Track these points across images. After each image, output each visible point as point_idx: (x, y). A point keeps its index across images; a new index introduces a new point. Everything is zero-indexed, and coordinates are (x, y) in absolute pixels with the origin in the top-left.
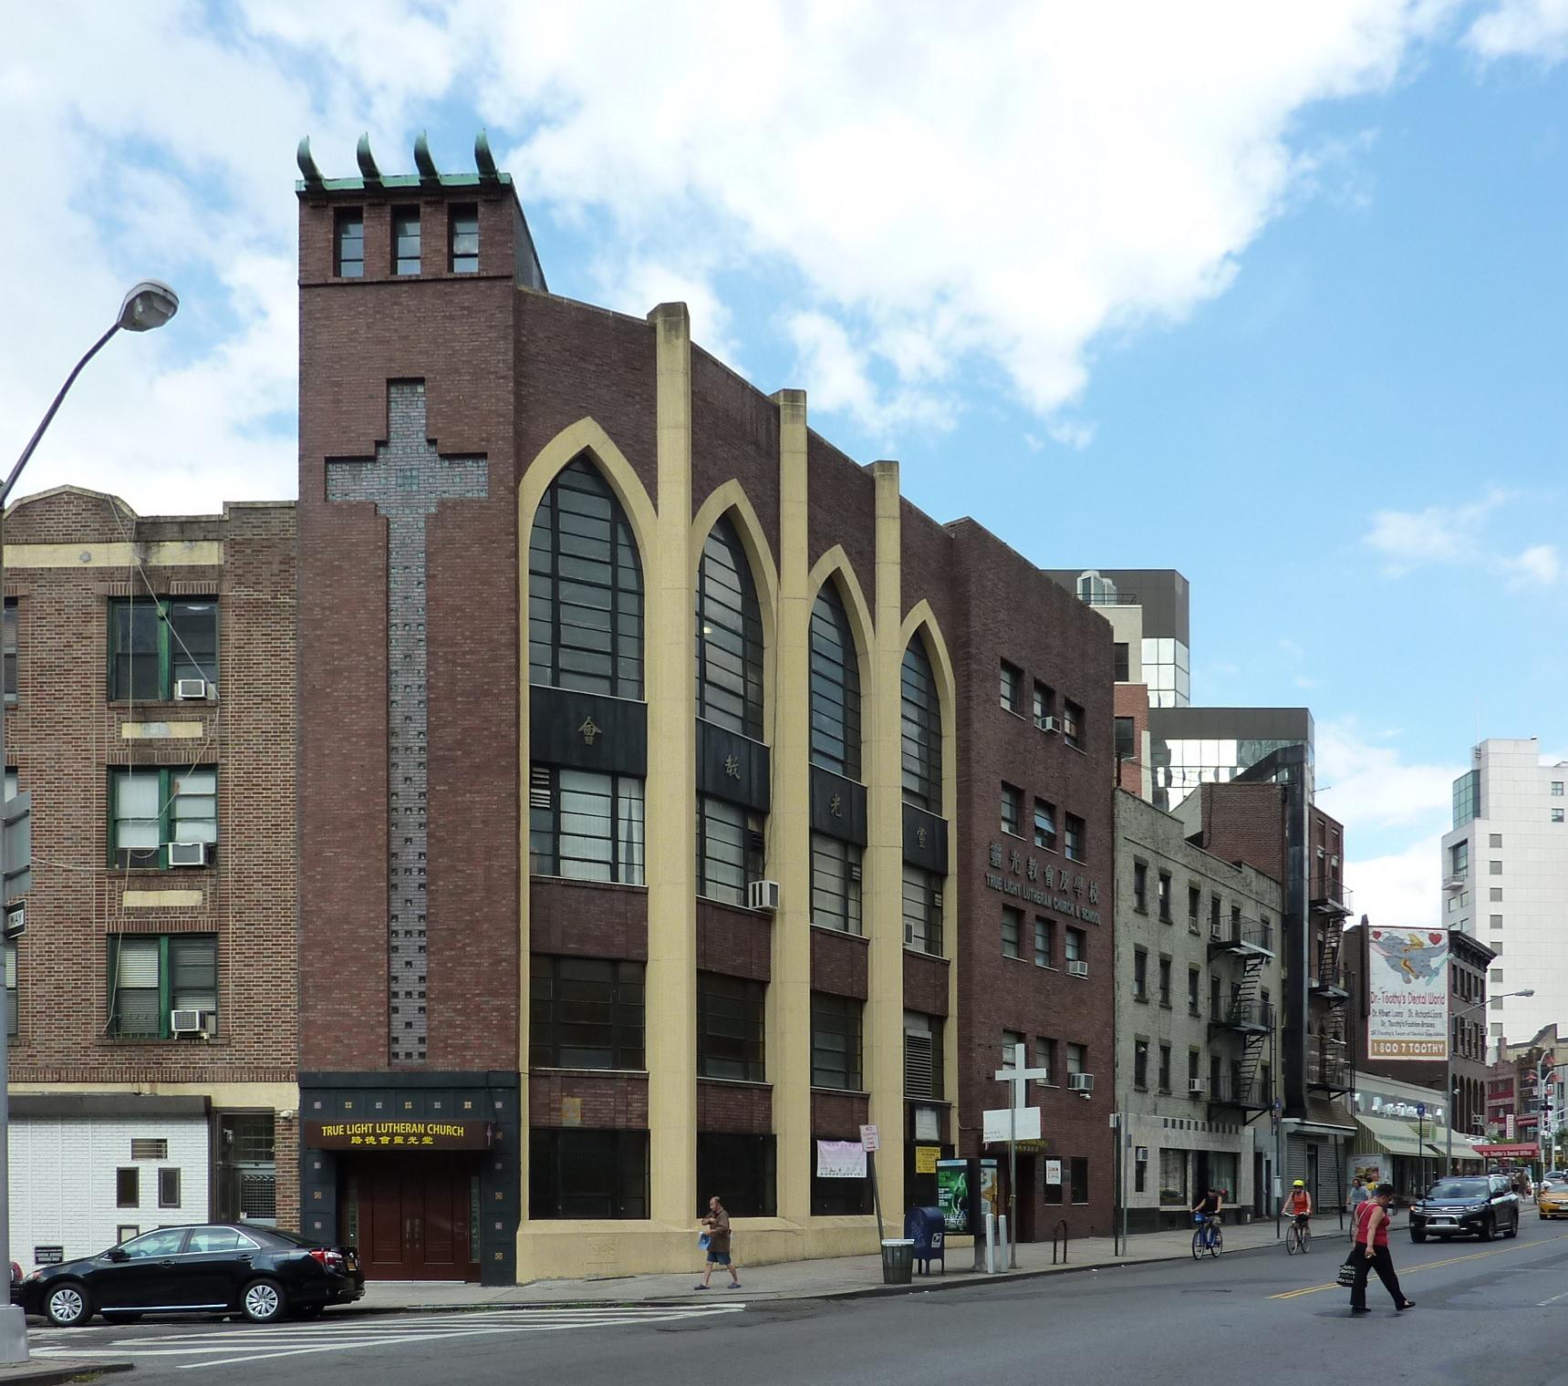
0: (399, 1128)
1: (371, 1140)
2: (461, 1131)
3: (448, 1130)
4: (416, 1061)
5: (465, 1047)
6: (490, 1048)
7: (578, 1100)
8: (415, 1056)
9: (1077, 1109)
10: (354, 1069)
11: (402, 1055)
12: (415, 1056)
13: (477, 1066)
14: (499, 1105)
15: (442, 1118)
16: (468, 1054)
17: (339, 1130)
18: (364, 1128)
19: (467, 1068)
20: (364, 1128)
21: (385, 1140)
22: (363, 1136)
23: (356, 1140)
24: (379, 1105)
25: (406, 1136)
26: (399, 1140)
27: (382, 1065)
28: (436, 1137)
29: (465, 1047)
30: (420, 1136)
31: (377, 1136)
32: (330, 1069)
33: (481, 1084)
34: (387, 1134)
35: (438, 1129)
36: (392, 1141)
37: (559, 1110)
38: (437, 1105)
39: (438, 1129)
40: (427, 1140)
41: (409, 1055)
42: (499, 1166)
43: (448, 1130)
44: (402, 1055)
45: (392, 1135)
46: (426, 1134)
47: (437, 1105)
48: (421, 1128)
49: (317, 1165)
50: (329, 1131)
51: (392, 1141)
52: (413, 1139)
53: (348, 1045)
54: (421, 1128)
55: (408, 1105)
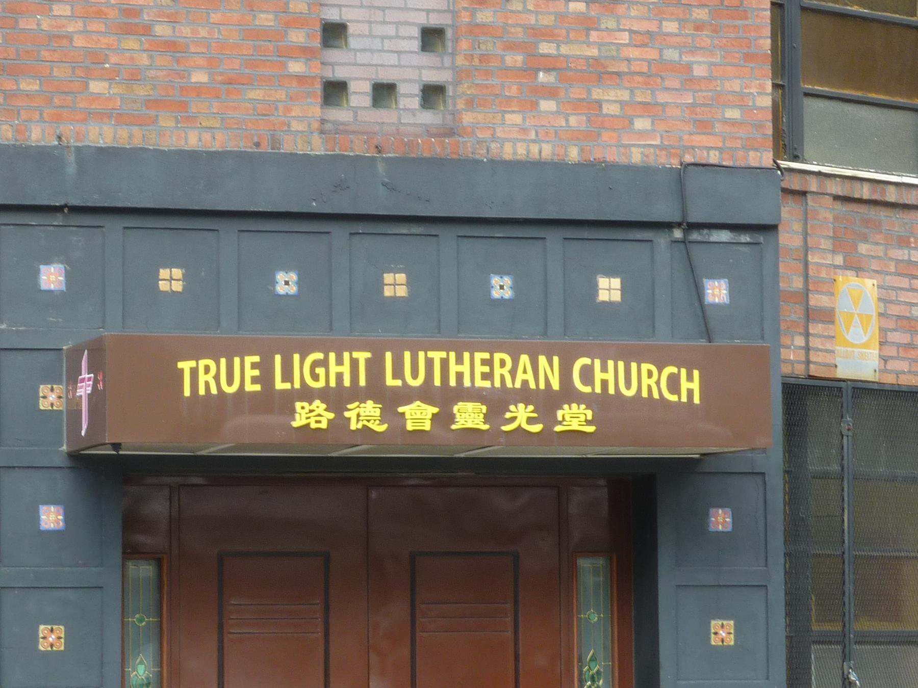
0: (468, 369)
1: (365, 415)
2: (692, 385)
3: (647, 380)
4: (409, 115)
5: (600, 72)
6: (689, 81)
7: (869, 285)
8: (409, 98)
9: (525, 395)
10: (193, 141)
11: (360, 93)
12: (409, 98)
13: (642, 144)
14: (717, 292)
15: (626, 334)
16: (612, 99)
17: (244, 374)
18: (339, 369)
19: (609, 151)
20: (339, 369)
21: (418, 416)
22: (337, 399)
23: (312, 415)
24: (286, 283)
25: (497, 402)
26: (469, 416)
27: (303, 128)
28: (604, 404)
29: (600, 72)
30: (547, 403)
31: (391, 401)
32: (100, 135)
33: (663, 211)
34: (426, 394)
35: (609, 375)
36: (444, 418)
37: (828, 316)
38: (501, 287)
39: (609, 375)
40: (574, 418)
41: (384, 92)
42: (721, 520)
43: (647, 380)
44: (360, 93)
45: (445, 397)
46: (568, 394)
47: (501, 287)
48: (549, 372)
49: (51, 518)
50: (205, 376)
51: (444, 418)
52: (521, 415)
53: (171, 46)
54: (549, 372)
55: (395, 285)
